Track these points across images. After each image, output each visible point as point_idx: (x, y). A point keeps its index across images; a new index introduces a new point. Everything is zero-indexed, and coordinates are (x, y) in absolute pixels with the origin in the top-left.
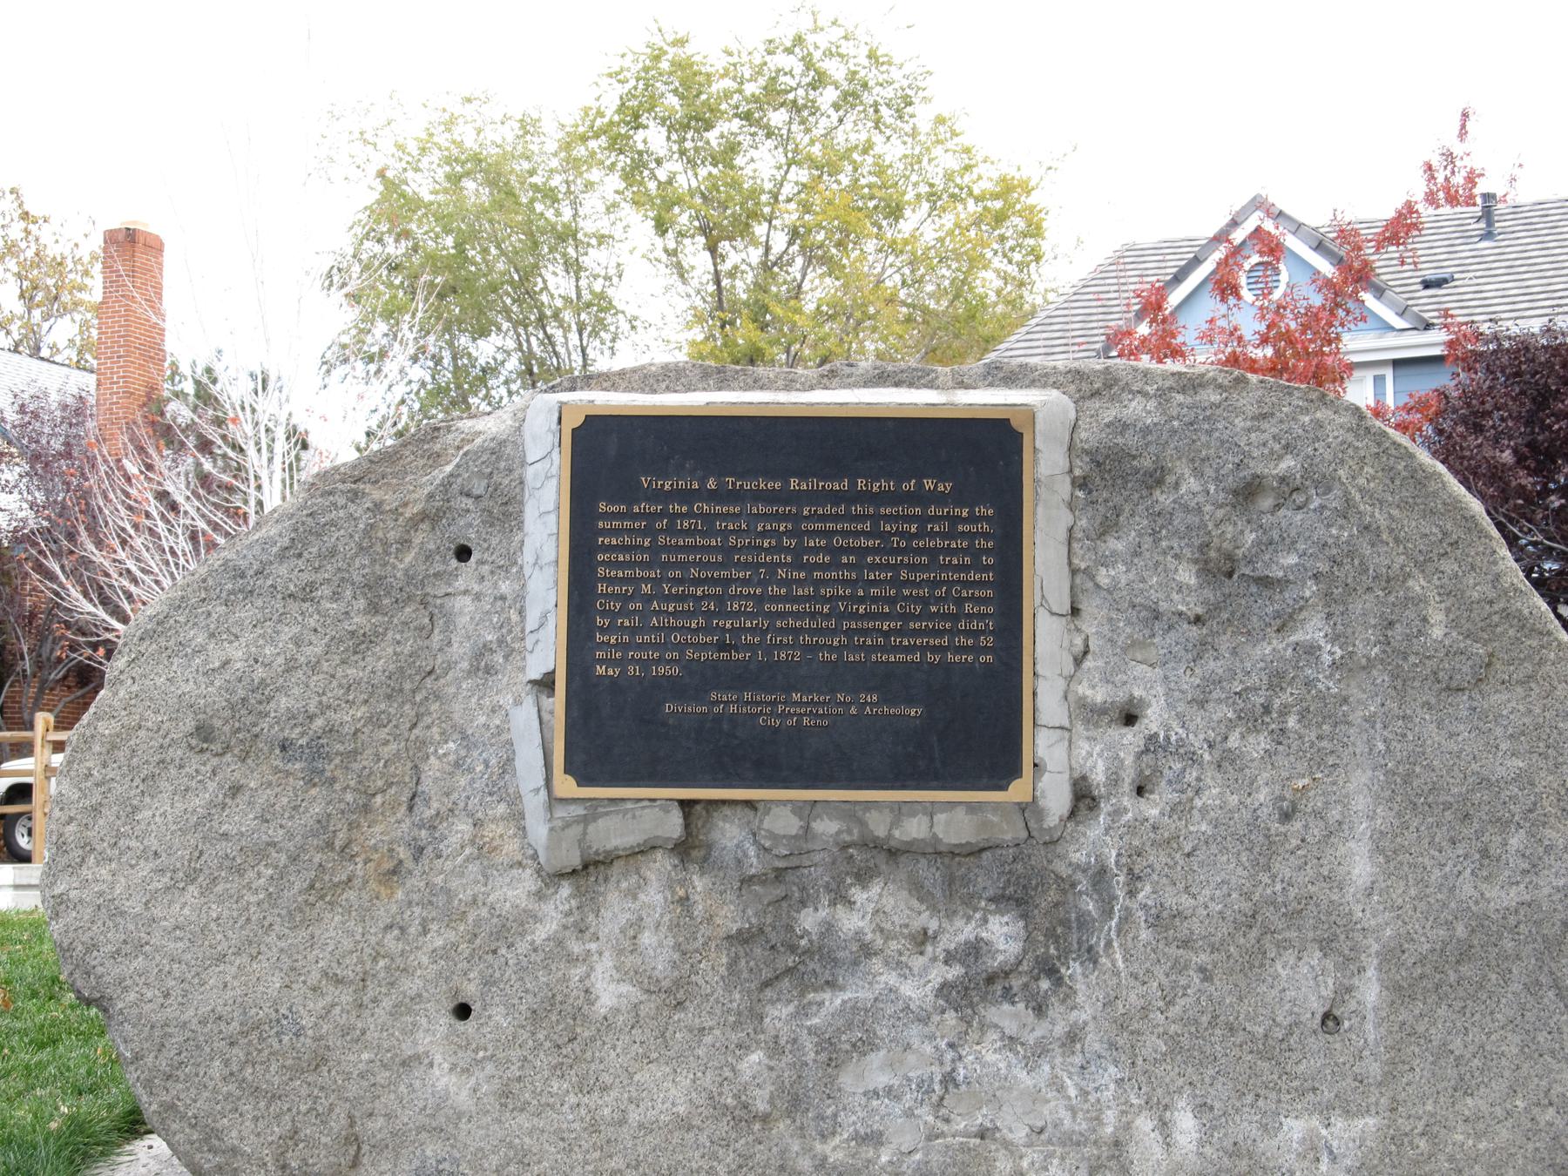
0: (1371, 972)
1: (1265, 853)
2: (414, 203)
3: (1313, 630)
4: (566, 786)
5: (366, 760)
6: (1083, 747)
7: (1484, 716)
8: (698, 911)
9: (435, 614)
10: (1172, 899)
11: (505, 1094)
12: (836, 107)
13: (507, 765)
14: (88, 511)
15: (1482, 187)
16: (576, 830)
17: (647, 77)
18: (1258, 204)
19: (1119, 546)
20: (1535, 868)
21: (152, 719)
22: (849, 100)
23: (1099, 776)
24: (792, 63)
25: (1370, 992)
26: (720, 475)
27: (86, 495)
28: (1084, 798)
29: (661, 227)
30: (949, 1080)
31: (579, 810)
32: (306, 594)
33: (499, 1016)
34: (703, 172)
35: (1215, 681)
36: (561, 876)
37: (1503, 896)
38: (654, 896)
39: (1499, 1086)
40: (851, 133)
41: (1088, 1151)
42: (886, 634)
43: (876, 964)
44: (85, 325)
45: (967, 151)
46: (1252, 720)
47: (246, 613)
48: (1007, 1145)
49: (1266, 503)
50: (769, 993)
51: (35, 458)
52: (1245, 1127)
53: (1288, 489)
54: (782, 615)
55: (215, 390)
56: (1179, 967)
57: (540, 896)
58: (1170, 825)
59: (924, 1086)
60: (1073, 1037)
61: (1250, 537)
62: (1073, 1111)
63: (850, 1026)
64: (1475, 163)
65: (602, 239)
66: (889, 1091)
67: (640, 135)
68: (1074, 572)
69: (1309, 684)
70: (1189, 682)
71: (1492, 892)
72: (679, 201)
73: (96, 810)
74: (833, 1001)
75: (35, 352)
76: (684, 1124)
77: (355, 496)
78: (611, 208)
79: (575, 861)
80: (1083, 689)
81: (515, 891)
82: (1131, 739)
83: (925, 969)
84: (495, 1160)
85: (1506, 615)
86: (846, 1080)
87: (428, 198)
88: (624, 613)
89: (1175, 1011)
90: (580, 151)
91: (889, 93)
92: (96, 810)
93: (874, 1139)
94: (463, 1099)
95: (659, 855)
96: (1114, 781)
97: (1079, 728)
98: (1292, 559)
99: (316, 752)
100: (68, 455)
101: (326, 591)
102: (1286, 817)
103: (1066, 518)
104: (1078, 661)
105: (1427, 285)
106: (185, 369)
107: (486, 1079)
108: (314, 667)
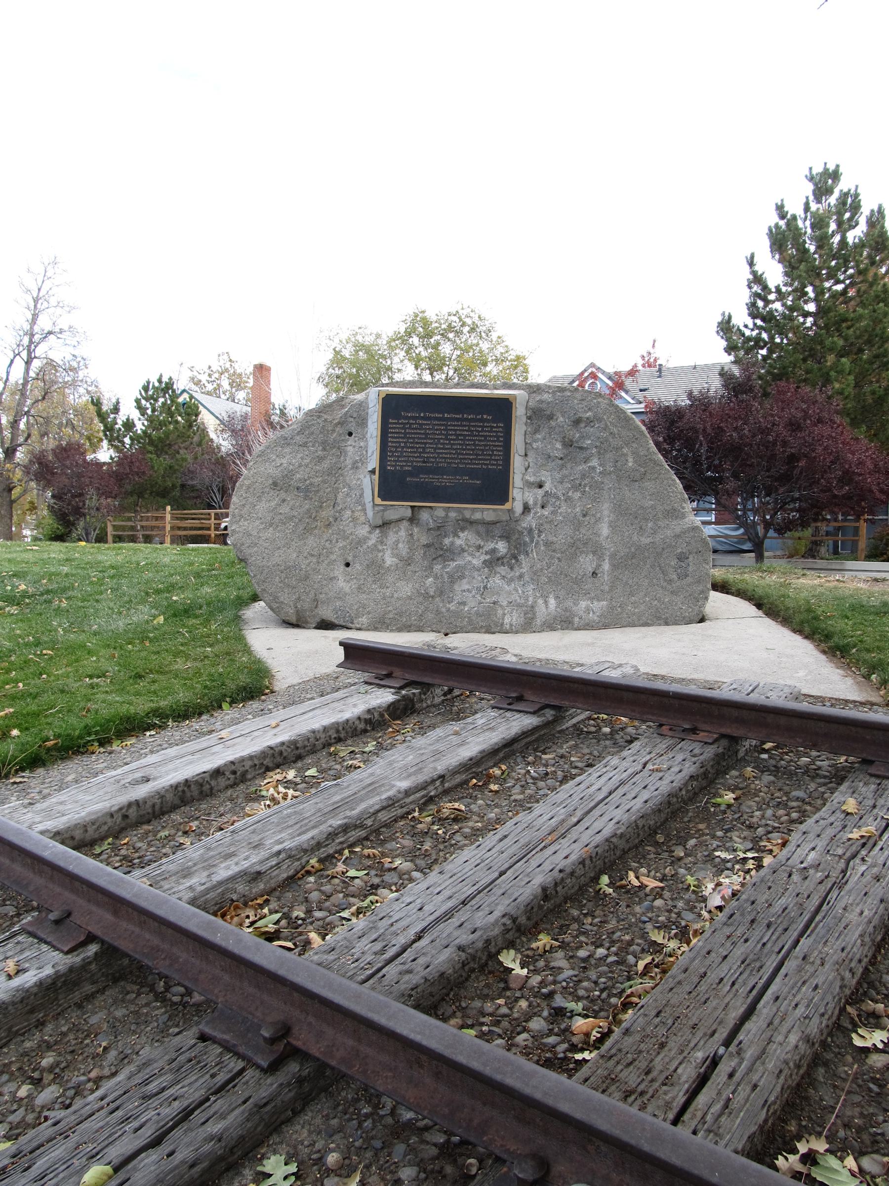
0: (607, 561)
1: (578, 526)
2: (344, 358)
3: (594, 462)
4: (378, 501)
5: (321, 493)
6: (527, 494)
7: (642, 489)
8: (415, 538)
9: (342, 452)
10: (551, 538)
11: (359, 588)
12: (469, 332)
13: (362, 495)
14: (248, 446)
15: (659, 362)
16: (381, 513)
17: (413, 321)
18: (592, 365)
19: (540, 437)
20: (655, 533)
21: (260, 480)
22: (472, 330)
23: (531, 502)
24: (455, 319)
25: (606, 566)
26: (425, 413)
27: (248, 441)
28: (526, 509)
29: (416, 368)
30: (485, 587)
31: (381, 508)
32: (305, 445)
33: (358, 566)
34: (429, 351)
35: (565, 476)
36: (377, 527)
37: (645, 540)
38: (403, 533)
39: (642, 594)
40: (473, 340)
41: (524, 608)
42: (471, 460)
43: (466, 554)
44: (248, 393)
45: (507, 346)
46: (576, 488)
47: (287, 450)
48: (501, 606)
49: (582, 425)
50: (435, 562)
51: (233, 431)
52: (569, 603)
53: (589, 421)
54: (442, 453)
55: (286, 411)
56: (552, 557)
57: (370, 532)
58: (551, 517)
59: (478, 589)
60: (521, 576)
61: (578, 435)
62: (520, 597)
63: (457, 571)
64: (657, 355)
65: (399, 370)
66: (468, 590)
67: (411, 340)
68: (526, 444)
69: (593, 478)
70: (558, 476)
71: (643, 539)
72: (422, 360)
73: (244, 505)
74: (453, 564)
75: (233, 401)
76: (410, 598)
77: (319, 417)
78: (402, 361)
79: (380, 523)
80: (527, 477)
81: (363, 531)
82: (540, 492)
83: (480, 556)
84: (356, 607)
85: (650, 460)
86: (456, 587)
87: (348, 357)
88: (396, 451)
89: (550, 570)
90: (393, 344)
91: (484, 328)
92: (244, 505)
93: (464, 603)
94: (347, 589)
95: (404, 521)
96: (535, 504)
97: (526, 488)
98: (589, 442)
99: (307, 490)
100: (242, 430)
101: (311, 444)
102: (584, 516)
103: (524, 428)
104: (526, 469)
105: (641, 390)
106: (277, 406)
107: (354, 584)
108: (307, 466)
